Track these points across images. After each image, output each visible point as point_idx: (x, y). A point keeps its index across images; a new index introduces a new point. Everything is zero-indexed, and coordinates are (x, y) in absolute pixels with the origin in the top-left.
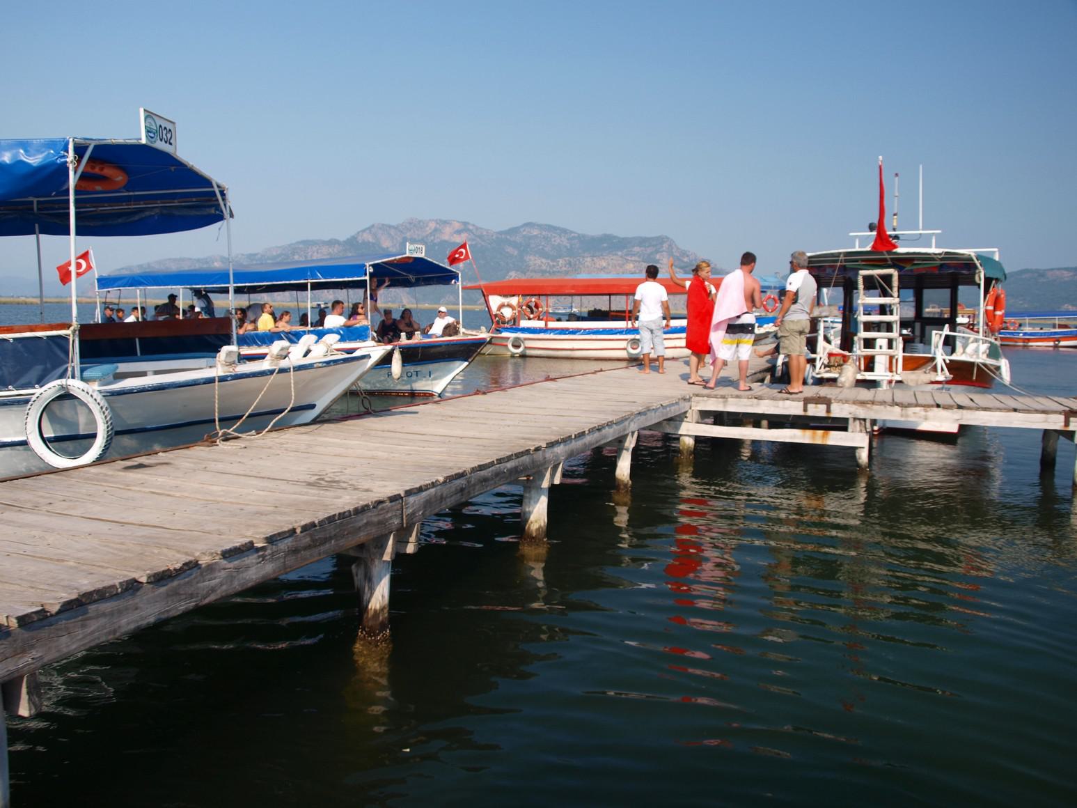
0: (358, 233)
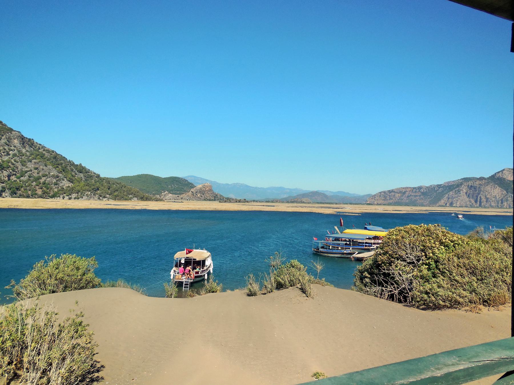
0: (496, 174)
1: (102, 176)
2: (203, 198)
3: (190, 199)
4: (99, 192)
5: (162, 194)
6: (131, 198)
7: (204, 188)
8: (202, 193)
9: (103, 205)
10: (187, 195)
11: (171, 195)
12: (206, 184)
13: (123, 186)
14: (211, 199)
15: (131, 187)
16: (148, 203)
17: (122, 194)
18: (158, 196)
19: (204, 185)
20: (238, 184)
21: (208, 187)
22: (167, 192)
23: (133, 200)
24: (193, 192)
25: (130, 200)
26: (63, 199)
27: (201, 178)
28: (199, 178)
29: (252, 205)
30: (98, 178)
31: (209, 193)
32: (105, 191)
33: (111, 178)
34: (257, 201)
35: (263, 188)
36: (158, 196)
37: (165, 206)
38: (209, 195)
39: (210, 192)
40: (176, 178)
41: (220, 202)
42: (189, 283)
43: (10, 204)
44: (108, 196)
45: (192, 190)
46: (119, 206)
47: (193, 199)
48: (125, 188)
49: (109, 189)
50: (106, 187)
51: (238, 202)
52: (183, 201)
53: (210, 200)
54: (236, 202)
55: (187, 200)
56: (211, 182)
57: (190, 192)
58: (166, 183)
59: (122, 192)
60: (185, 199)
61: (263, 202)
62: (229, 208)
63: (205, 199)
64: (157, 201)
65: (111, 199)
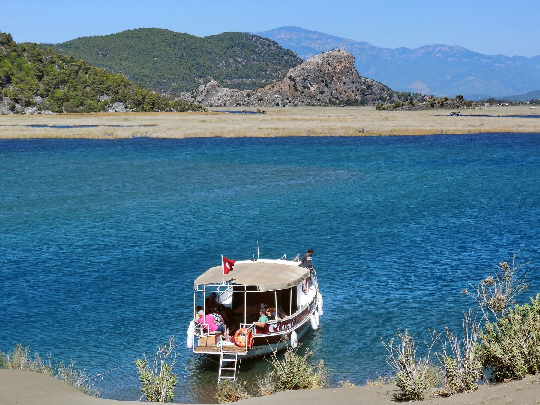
1: (18, 39)
2: (326, 98)
3: (285, 101)
4: (11, 87)
5: (201, 88)
6: (106, 104)
7: (329, 64)
8: (323, 81)
9: (23, 128)
11: (226, 90)
12: (335, 53)
13: (80, 68)
14: (352, 101)
15: (105, 69)
16: (154, 117)
17: (80, 93)
18: (187, 97)
19: (329, 56)
20: (439, 48)
22: (213, 82)
23: (111, 111)
25: (104, 110)
27: (320, 34)
28: (314, 33)
29: (486, 114)
30: (7, 47)
31: (344, 79)
32: (28, 86)
33: (46, 45)
34: (500, 102)
35: (521, 59)
36: (187, 97)
37: (205, 125)
38: (345, 88)
39: (346, 76)
40: (240, 35)
41: (379, 108)
42: (236, 360)
44: (38, 99)
45: (292, 73)
46: (70, 129)
47: (296, 102)
48: (86, 73)
49: (40, 78)
50: (32, 73)
51: (438, 108)
52: (262, 109)
53: (348, 103)
54: (432, 106)
55: (278, 105)
56: (352, 44)
57: (286, 80)
58: (210, 52)
59: (79, 87)
60: (270, 102)
61: (521, 103)
62: (405, 128)
63: (334, 100)
64: (183, 110)
65: (48, 109)
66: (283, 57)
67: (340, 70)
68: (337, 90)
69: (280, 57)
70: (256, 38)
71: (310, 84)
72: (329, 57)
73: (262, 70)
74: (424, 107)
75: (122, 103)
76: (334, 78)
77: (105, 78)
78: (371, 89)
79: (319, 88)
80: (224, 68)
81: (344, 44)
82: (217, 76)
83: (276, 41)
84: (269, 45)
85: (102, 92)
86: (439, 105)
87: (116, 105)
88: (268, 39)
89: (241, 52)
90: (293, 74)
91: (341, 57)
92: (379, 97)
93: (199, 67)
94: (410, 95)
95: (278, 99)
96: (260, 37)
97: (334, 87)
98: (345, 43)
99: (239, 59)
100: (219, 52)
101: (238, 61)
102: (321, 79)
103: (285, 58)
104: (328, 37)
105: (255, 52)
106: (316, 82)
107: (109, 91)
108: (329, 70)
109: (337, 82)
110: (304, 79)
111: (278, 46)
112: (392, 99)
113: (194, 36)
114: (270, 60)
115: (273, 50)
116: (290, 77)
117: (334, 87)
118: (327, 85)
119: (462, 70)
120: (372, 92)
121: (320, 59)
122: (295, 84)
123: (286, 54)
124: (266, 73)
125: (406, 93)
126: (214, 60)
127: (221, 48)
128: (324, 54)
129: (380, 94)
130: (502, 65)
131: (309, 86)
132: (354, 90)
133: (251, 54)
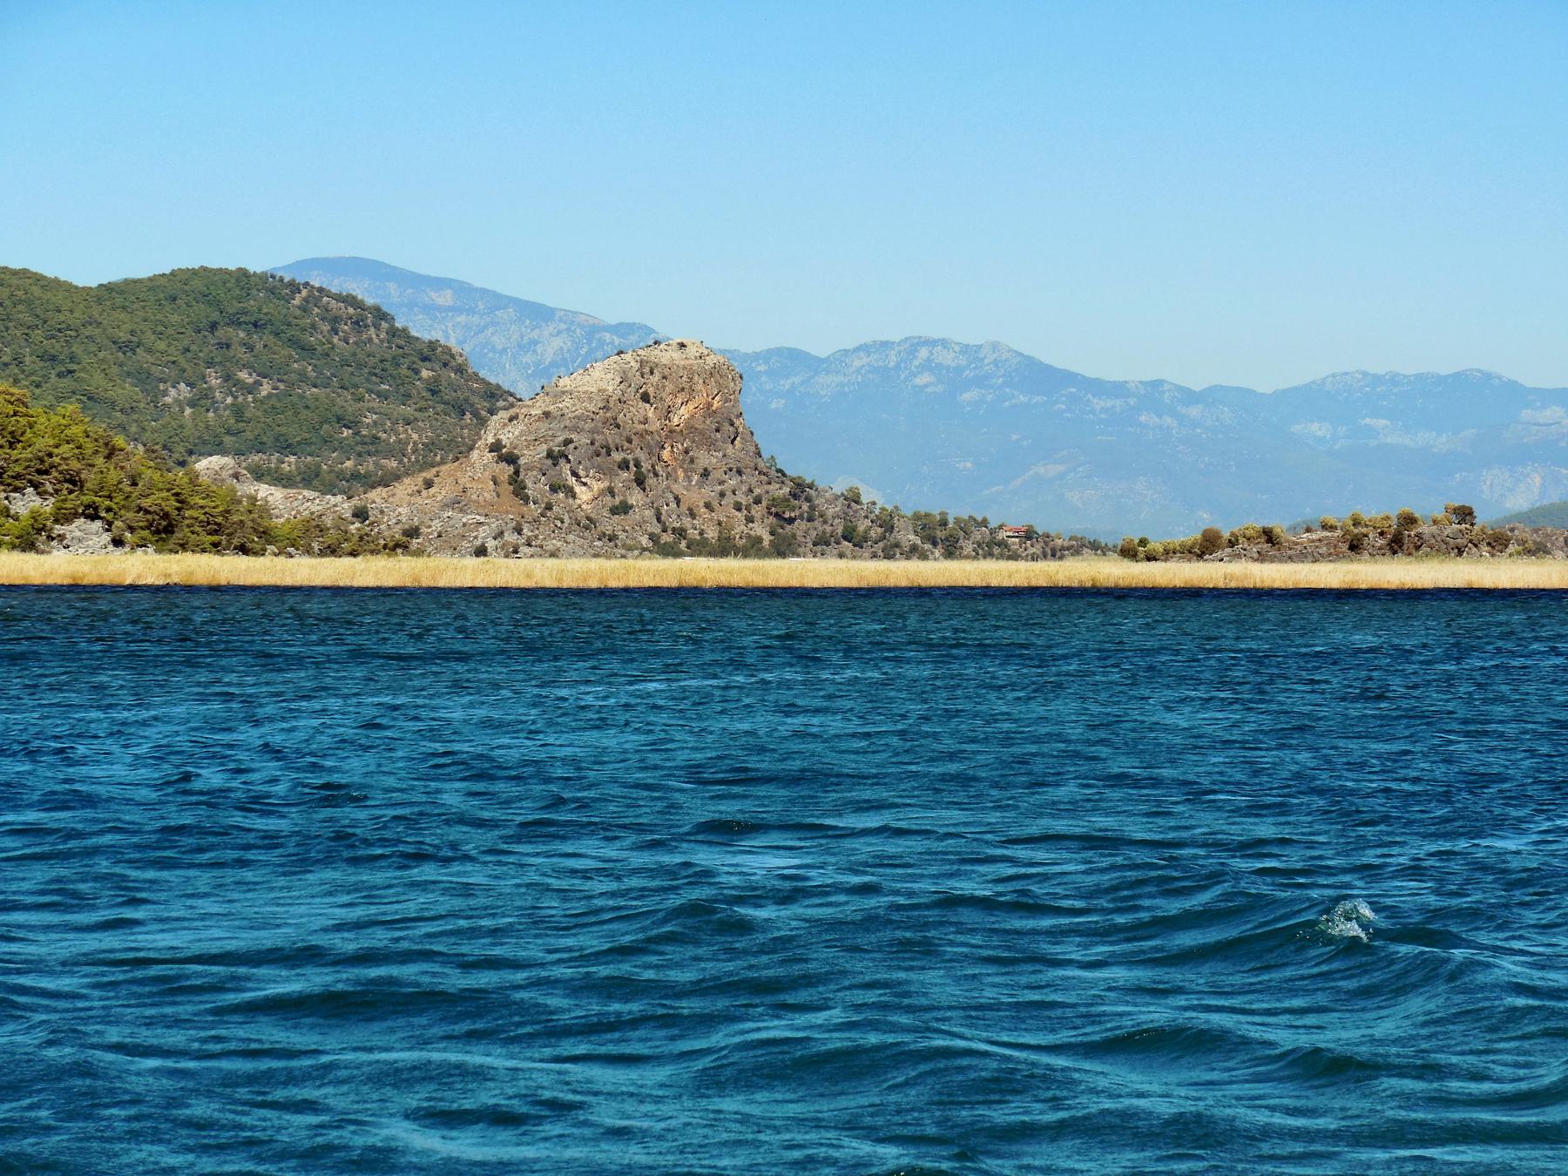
3: (510, 537)
7: (645, 398)
8: (624, 465)
10: (442, 492)
19: (647, 368)
20: (923, 353)
21: (688, 390)
24: (511, 459)
26: (706, 470)
27: (462, 289)
28: (440, 283)
31: (704, 459)
35: (1244, 398)
38: (709, 492)
39: (711, 445)
43: (1467, 577)
45: (500, 429)
55: (481, 552)
57: (481, 457)
58: (127, 347)
63: (667, 538)
66: (417, 372)
67: (687, 422)
68: (678, 500)
69: (404, 371)
70: (304, 293)
71: (575, 474)
72: (647, 370)
73: (339, 419)
74: (1323, 550)
75: (98, 524)
76: (666, 454)
77: (23, 421)
78: (808, 499)
79: (611, 491)
80: (188, 411)
81: (559, 333)
82: (162, 439)
83: (385, 308)
84: (357, 323)
85: (17, 477)
86: (1381, 542)
87: (78, 534)
88: (354, 298)
89: (251, 348)
90: (509, 436)
91: (688, 369)
92: (840, 530)
93: (90, 404)
94: (944, 523)
95: (483, 532)
96: (321, 290)
97: (668, 487)
98: (563, 326)
99: (243, 375)
100: (162, 346)
101: (238, 383)
102: (617, 456)
103: (425, 374)
104: (497, 301)
105: (307, 350)
106: (600, 469)
107: (46, 472)
108: (645, 421)
109: (675, 470)
110: (550, 455)
111: (392, 326)
112: (892, 539)
113: (56, 281)
114: (368, 380)
115: (376, 341)
116: (496, 447)
117: (668, 487)
118: (640, 481)
119: (1015, 437)
120: (812, 508)
121: (610, 376)
122: (517, 473)
123: (425, 359)
124: (357, 433)
125: (927, 515)
126: (143, 377)
127: (170, 331)
128: (628, 357)
129: (845, 516)
130: (1168, 420)
131: (572, 481)
132: (742, 499)
133: (290, 357)
